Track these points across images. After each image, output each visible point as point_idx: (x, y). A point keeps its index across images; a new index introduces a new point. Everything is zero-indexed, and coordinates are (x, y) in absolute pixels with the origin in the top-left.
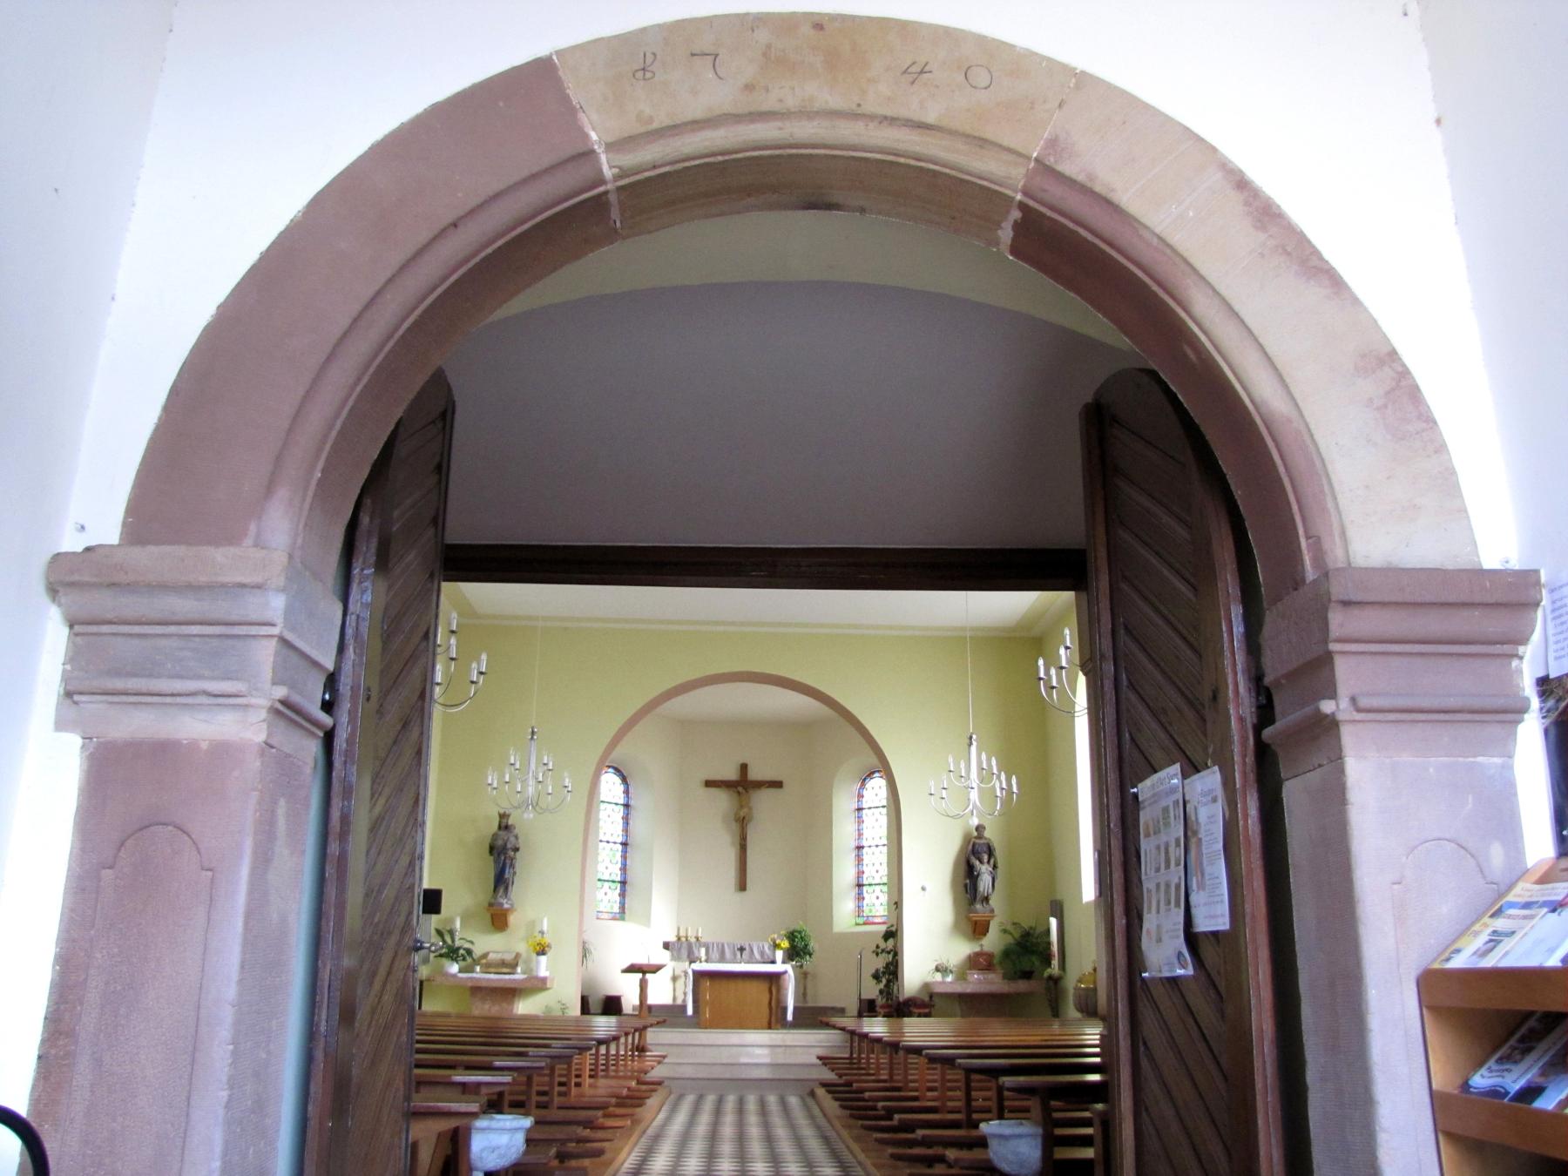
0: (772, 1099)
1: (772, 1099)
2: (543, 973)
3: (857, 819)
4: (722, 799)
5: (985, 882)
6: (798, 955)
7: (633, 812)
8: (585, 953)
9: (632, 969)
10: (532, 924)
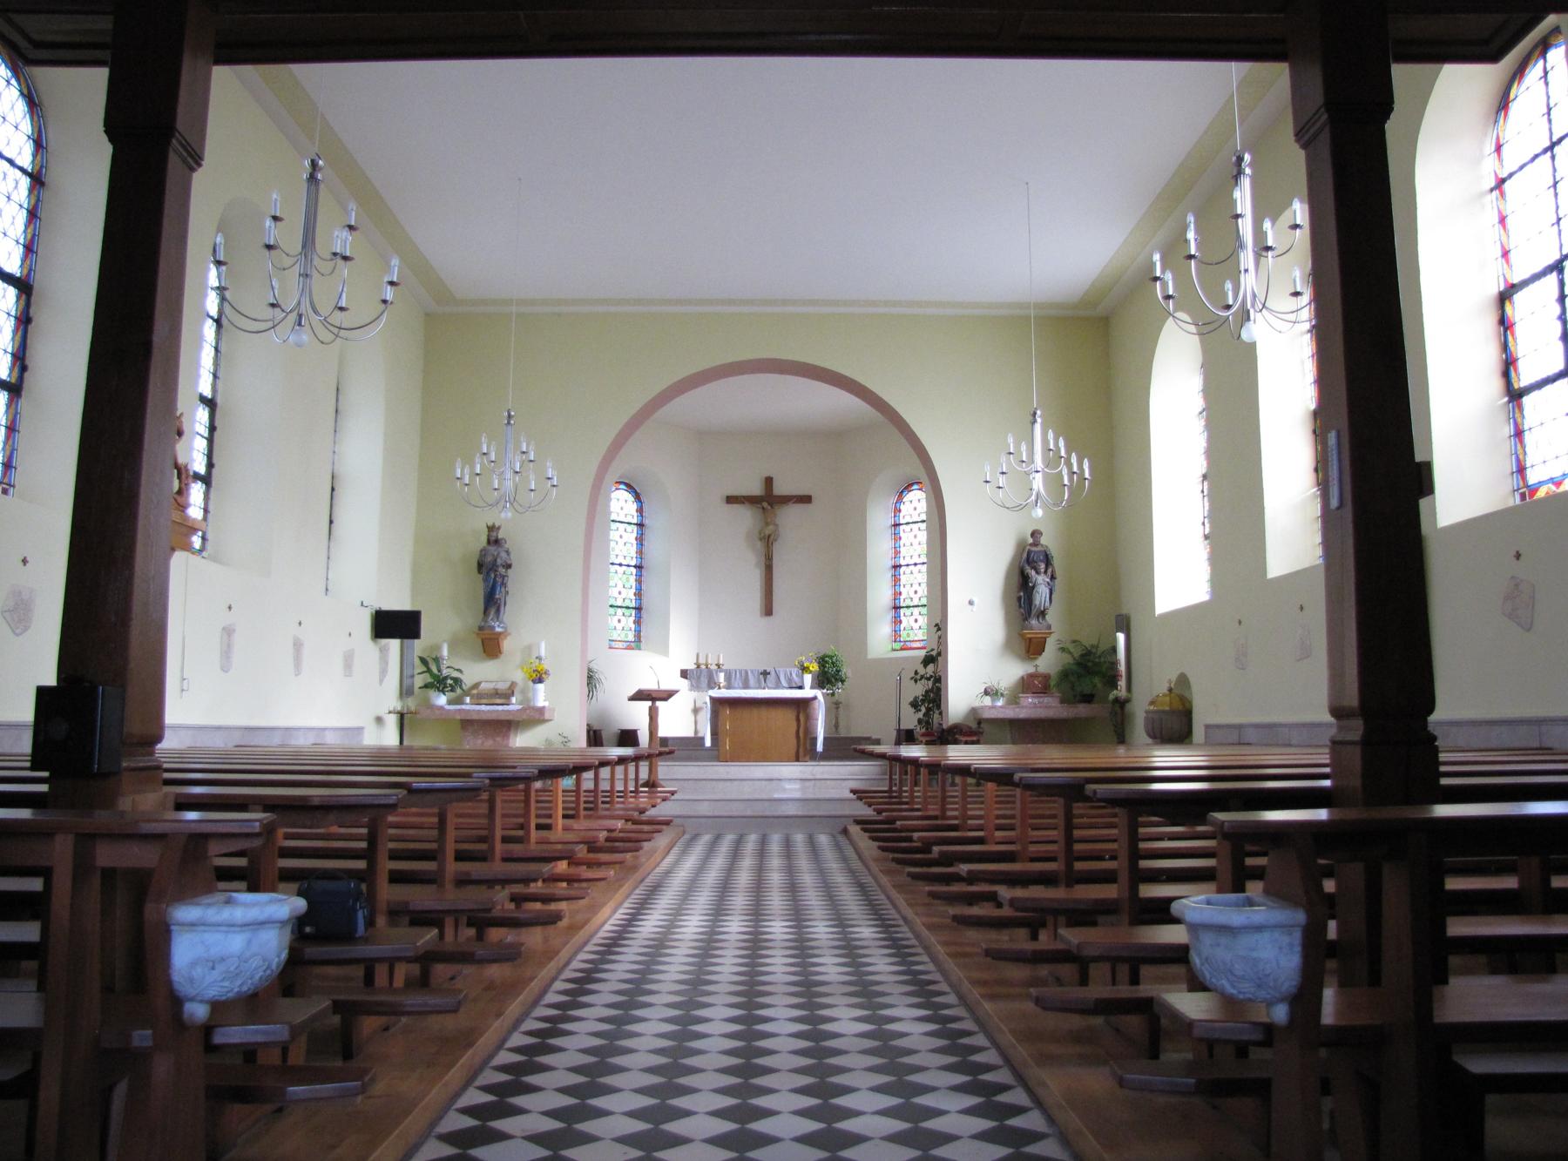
0: (799, 839)
1: (799, 839)
2: (541, 702)
3: (895, 536)
4: (745, 517)
5: (1041, 594)
6: (829, 682)
7: (647, 531)
8: (591, 680)
9: (640, 696)
10: (529, 649)
